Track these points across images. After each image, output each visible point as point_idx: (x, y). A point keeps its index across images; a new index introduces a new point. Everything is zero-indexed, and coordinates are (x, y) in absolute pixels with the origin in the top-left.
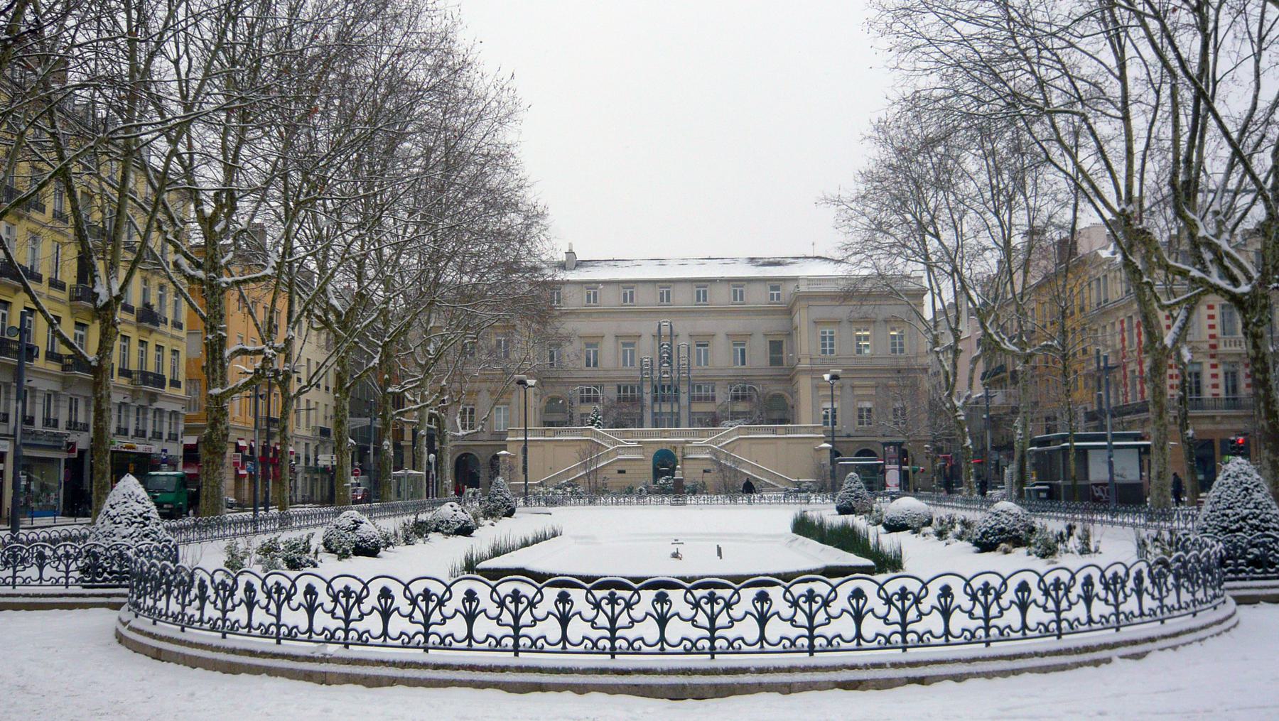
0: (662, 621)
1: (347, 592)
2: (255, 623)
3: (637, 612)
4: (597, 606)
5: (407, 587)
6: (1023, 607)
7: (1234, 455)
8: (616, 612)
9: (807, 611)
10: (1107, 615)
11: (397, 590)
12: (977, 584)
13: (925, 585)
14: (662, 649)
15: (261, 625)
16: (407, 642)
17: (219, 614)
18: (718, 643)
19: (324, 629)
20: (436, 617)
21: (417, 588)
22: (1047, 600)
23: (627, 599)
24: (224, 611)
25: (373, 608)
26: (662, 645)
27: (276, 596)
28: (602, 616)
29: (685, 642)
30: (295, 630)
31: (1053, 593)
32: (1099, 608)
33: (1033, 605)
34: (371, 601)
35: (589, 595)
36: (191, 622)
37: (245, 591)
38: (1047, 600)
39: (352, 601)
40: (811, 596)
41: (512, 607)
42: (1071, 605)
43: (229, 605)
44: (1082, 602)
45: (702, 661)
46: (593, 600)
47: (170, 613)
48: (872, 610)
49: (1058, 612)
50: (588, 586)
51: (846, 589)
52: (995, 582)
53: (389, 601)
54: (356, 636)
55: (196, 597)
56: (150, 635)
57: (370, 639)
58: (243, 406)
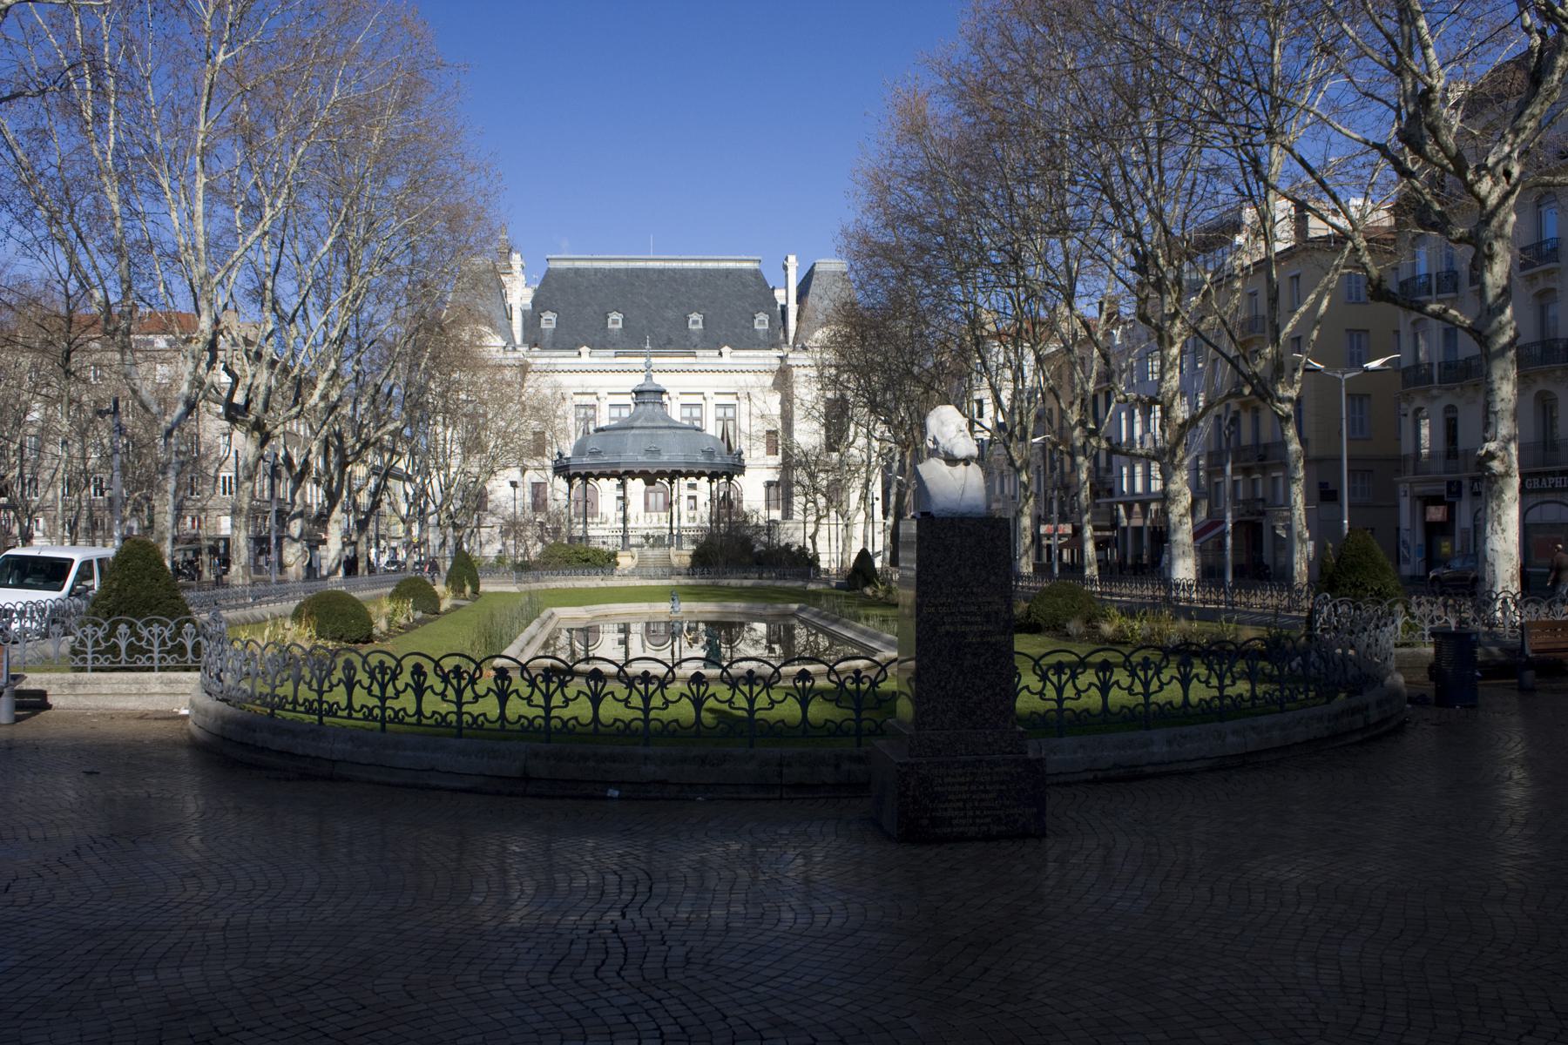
7: (924, 433)
8: (650, 691)
11: (428, 667)
15: (363, 706)
21: (448, 665)
28: (738, 695)
33: (514, 696)
34: (405, 678)
41: (543, 686)
42: (398, 694)
58: (833, 536)
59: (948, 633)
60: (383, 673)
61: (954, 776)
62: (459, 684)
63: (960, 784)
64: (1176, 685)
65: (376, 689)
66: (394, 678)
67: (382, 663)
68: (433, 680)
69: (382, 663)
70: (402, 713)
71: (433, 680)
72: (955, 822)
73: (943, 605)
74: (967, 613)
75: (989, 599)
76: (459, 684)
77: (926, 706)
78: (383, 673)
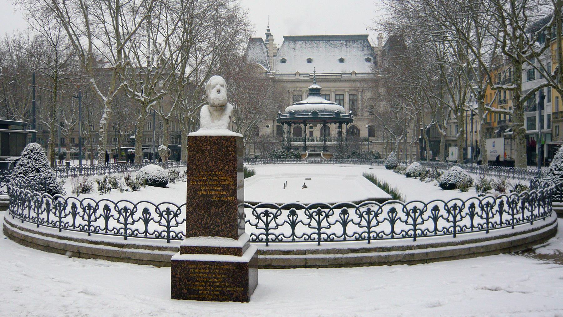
0: (293, 225)
1: (126, 209)
2: (77, 225)
3: (280, 220)
4: (258, 217)
5: (157, 207)
6: (435, 219)
9: (265, 221)
10: (482, 224)
11: (152, 209)
12: (450, 205)
13: (426, 206)
14: (294, 239)
15: (80, 225)
16: (447, 232)
17: (58, 219)
18: (270, 237)
19: (114, 228)
20: (374, 222)
21: (163, 208)
22: (482, 213)
23: (327, 213)
24: (60, 218)
25: (140, 218)
26: (345, 236)
27: (88, 211)
29: (305, 236)
30: (98, 228)
31: (453, 212)
32: (477, 220)
34: (100, 211)
35: (307, 211)
36: (42, 222)
37: (72, 207)
38: (482, 213)
39: (91, 211)
40: (369, 212)
42: (462, 218)
43: (63, 214)
44: (468, 216)
45: (313, 246)
46: (256, 214)
47: (31, 217)
48: (352, 220)
49: (455, 222)
50: (254, 207)
51: (386, 208)
52: (459, 204)
53: (108, 212)
54: (131, 232)
55: (45, 209)
56: (547, 225)
57: (138, 234)
59: (203, 195)
60: (90, 209)
61: (200, 269)
62: (168, 217)
63: (203, 273)
64: (431, 221)
65: (86, 217)
66: (95, 211)
67: (89, 204)
68: (114, 213)
69: (89, 204)
70: (98, 228)
71: (114, 213)
72: (200, 292)
73: (201, 180)
74: (213, 185)
75: (224, 178)
76: (168, 217)
77: (191, 232)
78: (90, 209)
